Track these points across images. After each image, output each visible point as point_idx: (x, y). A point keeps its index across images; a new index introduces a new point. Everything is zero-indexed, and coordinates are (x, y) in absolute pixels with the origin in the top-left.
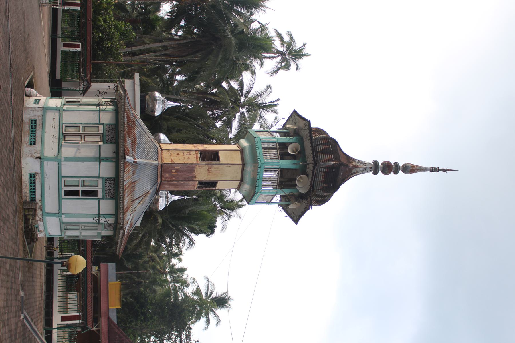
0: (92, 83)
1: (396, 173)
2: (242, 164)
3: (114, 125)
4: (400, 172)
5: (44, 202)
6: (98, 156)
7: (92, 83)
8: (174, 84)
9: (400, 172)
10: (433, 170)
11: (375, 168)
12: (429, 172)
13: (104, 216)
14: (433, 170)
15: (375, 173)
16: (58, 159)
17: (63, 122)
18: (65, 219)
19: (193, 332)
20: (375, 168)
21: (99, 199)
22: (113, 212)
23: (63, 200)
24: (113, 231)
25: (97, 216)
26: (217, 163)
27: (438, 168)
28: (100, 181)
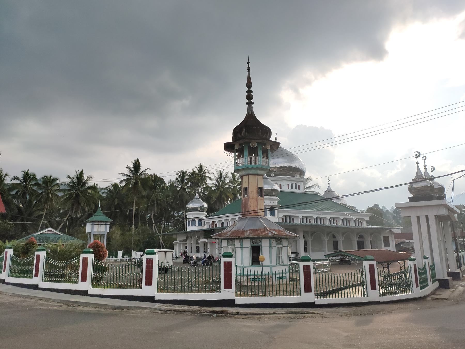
0: (94, 254)
1: (252, 92)
2: (249, 175)
3: (251, 240)
4: (251, 89)
5: (300, 271)
6: (269, 248)
7: (94, 254)
8: (12, 192)
9: (251, 89)
10: (249, 71)
11: (250, 104)
12: (250, 72)
13: (270, 244)
14: (249, 71)
15: (424, 166)
16: (270, 267)
17: (276, 264)
18: (274, 263)
19: (69, 177)
20: (250, 104)
21: (283, 247)
22: (268, 240)
23: (284, 264)
24: (243, 240)
25: (270, 248)
26: (248, 188)
27: (248, 67)
28: (277, 246)
